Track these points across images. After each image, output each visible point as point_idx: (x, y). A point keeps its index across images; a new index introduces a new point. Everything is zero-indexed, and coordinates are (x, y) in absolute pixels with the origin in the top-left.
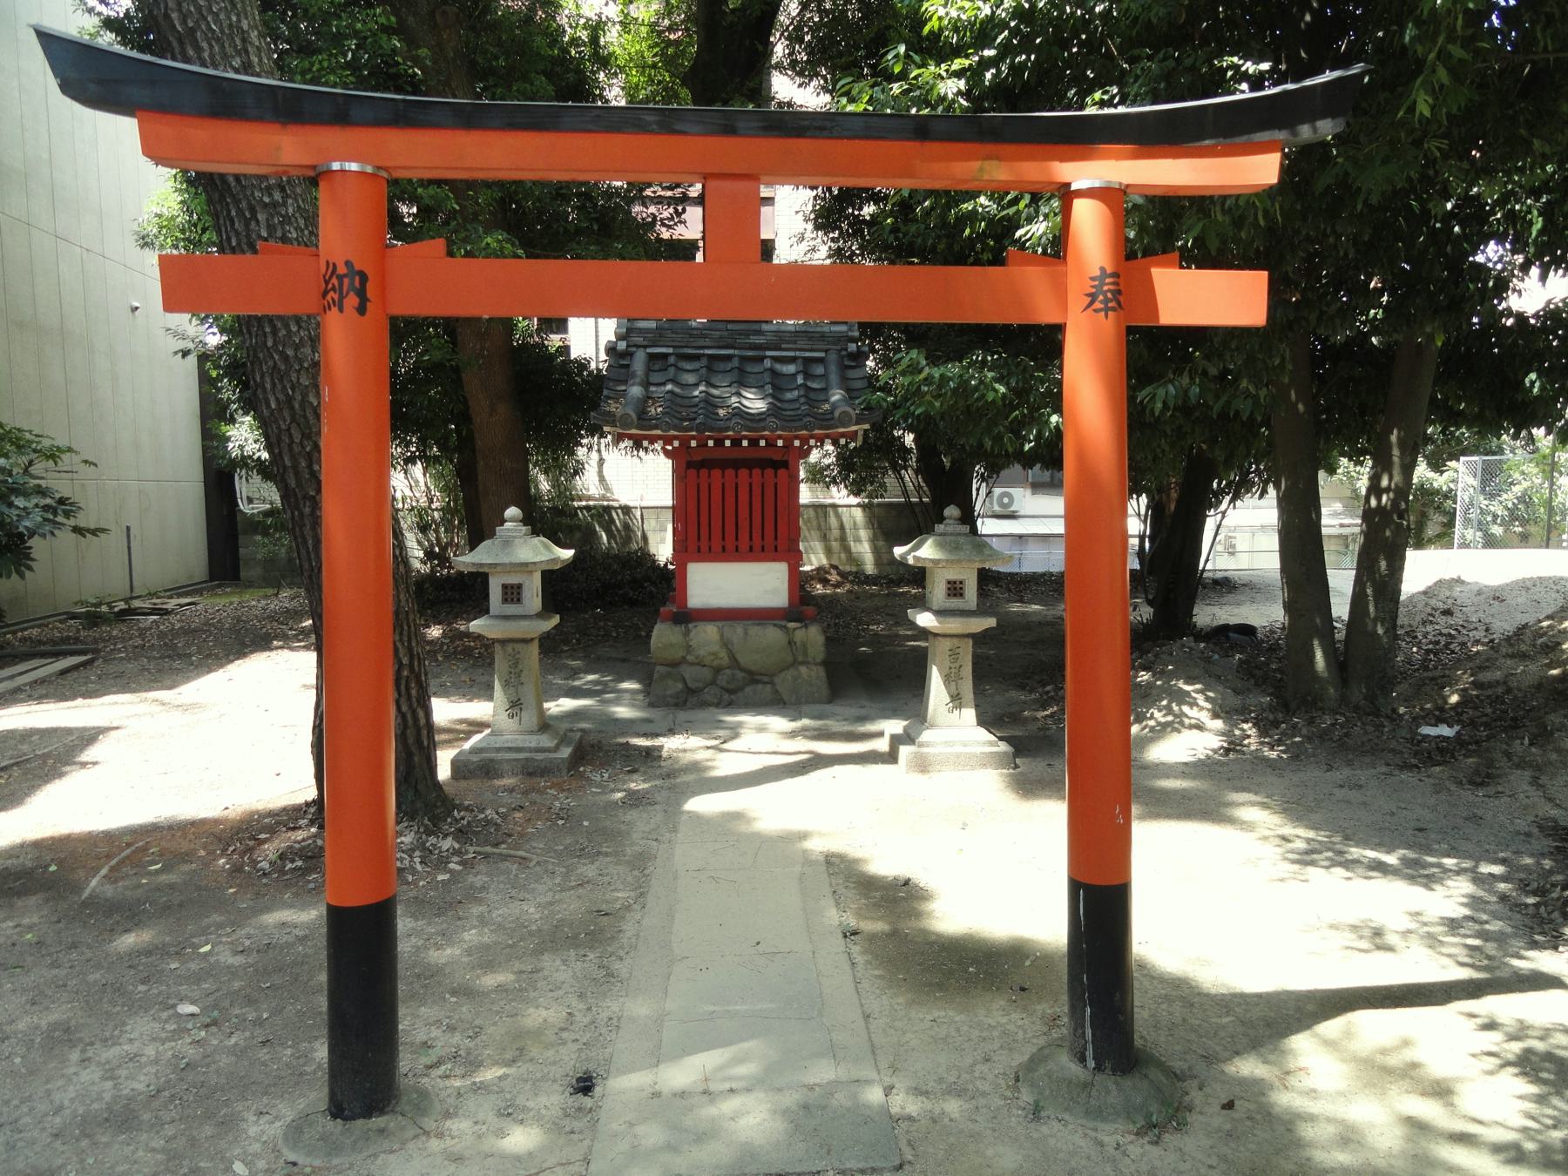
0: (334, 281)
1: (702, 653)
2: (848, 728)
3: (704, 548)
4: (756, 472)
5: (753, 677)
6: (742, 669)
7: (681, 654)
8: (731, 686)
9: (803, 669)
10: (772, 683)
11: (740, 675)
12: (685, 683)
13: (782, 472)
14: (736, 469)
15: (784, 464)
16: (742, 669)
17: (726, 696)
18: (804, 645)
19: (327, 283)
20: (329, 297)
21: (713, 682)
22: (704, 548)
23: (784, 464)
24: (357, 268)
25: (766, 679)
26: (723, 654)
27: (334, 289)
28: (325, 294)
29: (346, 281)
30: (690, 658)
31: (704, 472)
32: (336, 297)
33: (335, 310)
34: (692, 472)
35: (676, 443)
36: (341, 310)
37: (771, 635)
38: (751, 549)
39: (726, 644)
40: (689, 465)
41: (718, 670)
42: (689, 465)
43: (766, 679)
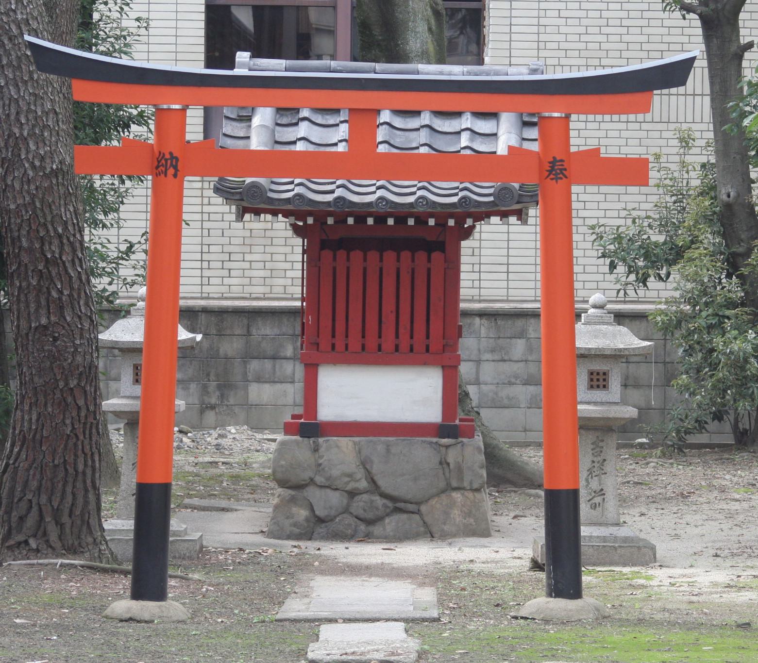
0: (163, 162)
1: (335, 472)
2: (305, 260)
3: (340, 346)
4: (406, 255)
5: (398, 505)
6: (384, 495)
7: (307, 475)
8: (370, 515)
9: (457, 495)
10: (418, 512)
11: (379, 501)
12: (312, 510)
13: (436, 255)
14: (381, 251)
15: (440, 246)
16: (384, 495)
17: (362, 527)
18: (459, 469)
19: (159, 162)
20: (159, 169)
21: (346, 510)
22: (340, 346)
23: (440, 246)
24: (174, 155)
25: (411, 507)
26: (360, 474)
27: (162, 165)
28: (157, 168)
29: (169, 162)
30: (319, 479)
31: (342, 254)
32: (164, 169)
33: (163, 176)
34: (327, 254)
35: (310, 221)
36: (166, 176)
37: (421, 453)
38: (397, 349)
39: (364, 464)
40: (324, 245)
41: (352, 494)
42: (324, 245)
43: (411, 507)
